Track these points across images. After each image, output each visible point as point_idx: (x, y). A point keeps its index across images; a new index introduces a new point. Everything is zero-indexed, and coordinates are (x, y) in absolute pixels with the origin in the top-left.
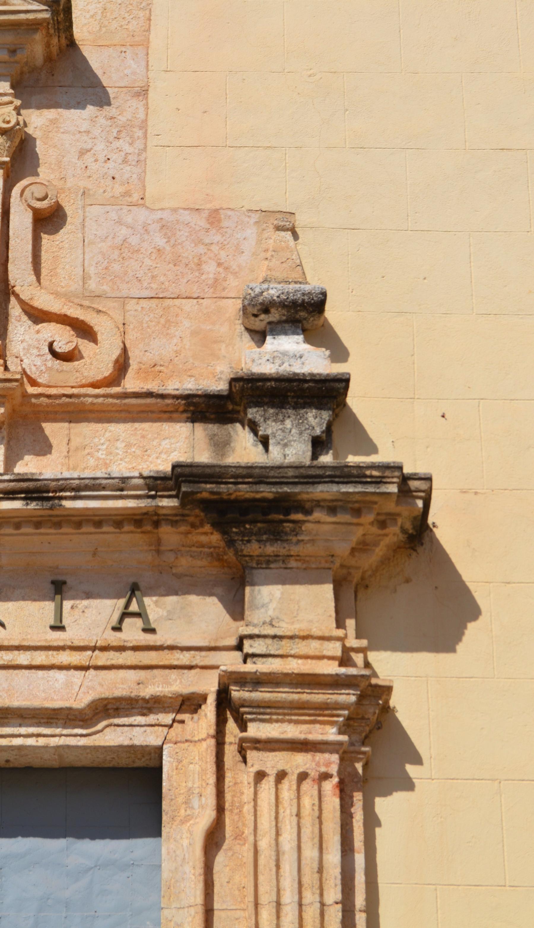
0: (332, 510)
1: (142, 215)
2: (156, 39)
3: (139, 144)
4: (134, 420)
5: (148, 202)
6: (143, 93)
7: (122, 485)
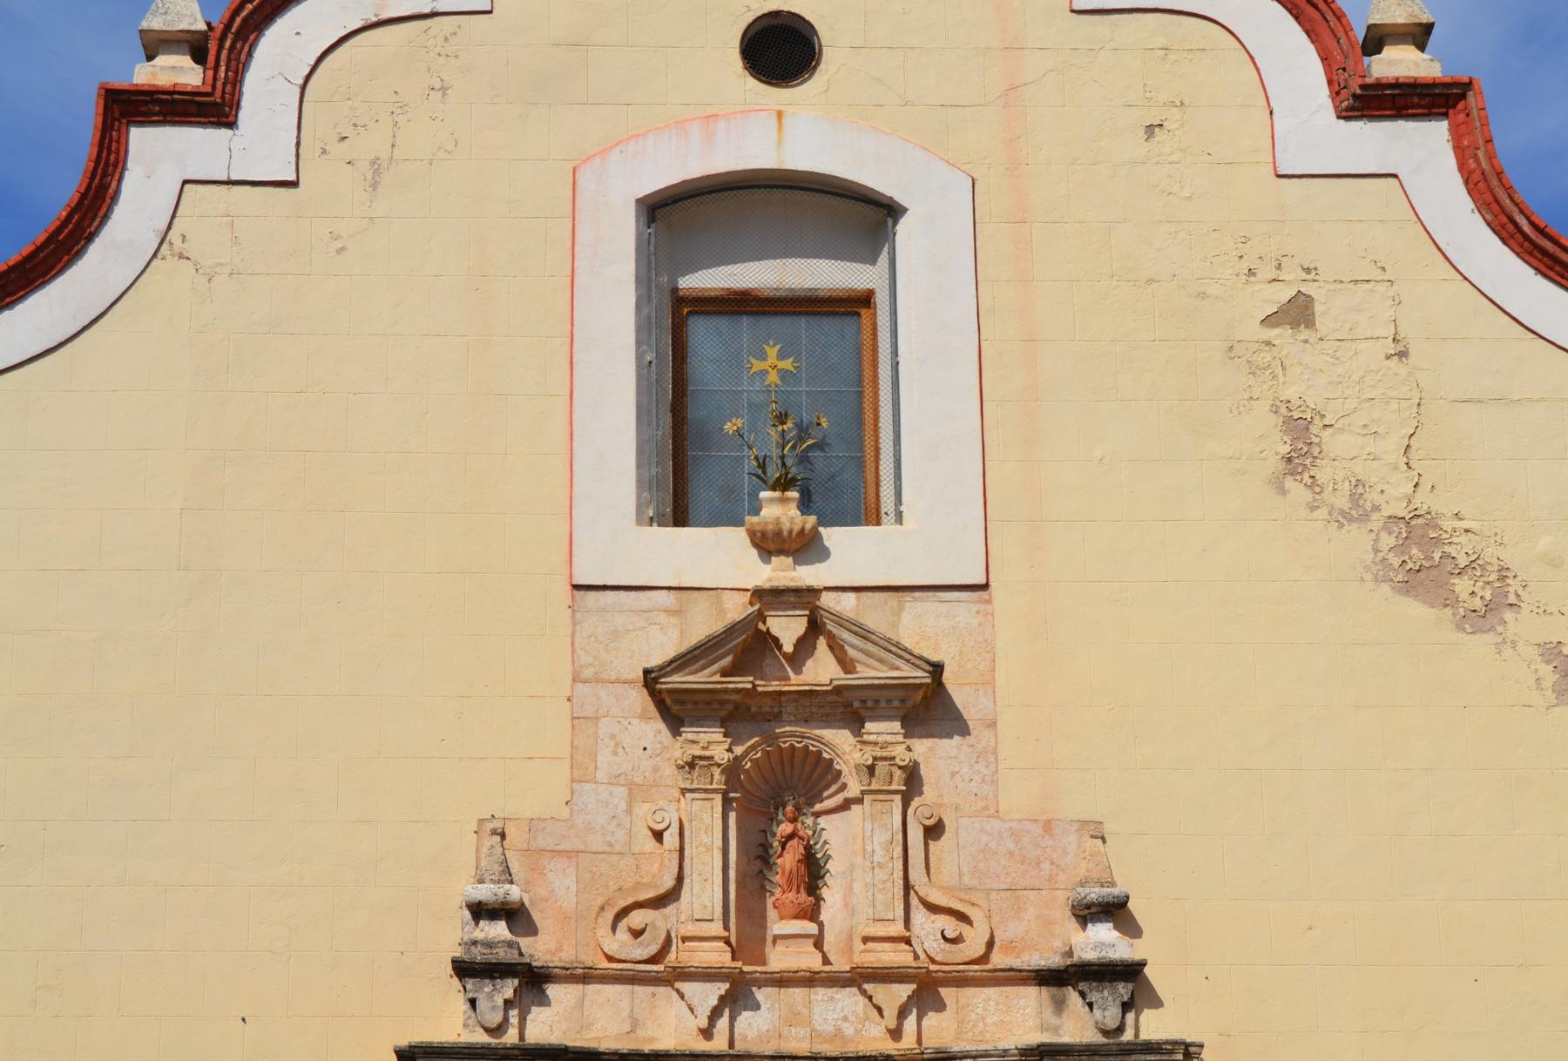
1: (996, 824)
2: (1000, 679)
4: (1000, 985)
5: (1001, 813)
6: (992, 725)
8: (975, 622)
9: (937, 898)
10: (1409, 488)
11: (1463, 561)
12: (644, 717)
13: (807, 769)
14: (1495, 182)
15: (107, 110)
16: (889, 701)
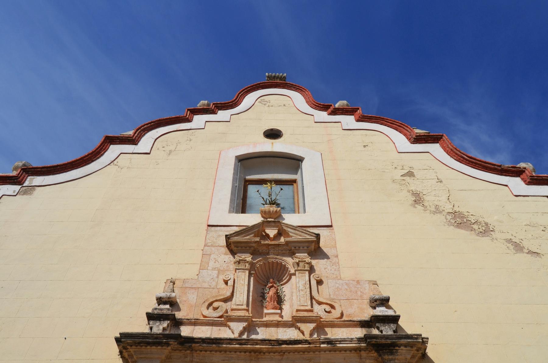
0: (406, 346)
1: (341, 281)
3: (338, 267)
4: (347, 327)
6: (337, 256)
7: (351, 340)
8: (329, 234)
9: (321, 300)
10: (452, 206)
11: (473, 222)
12: (226, 254)
13: (278, 271)
14: (455, 150)
15: (105, 139)
16: (303, 247)
